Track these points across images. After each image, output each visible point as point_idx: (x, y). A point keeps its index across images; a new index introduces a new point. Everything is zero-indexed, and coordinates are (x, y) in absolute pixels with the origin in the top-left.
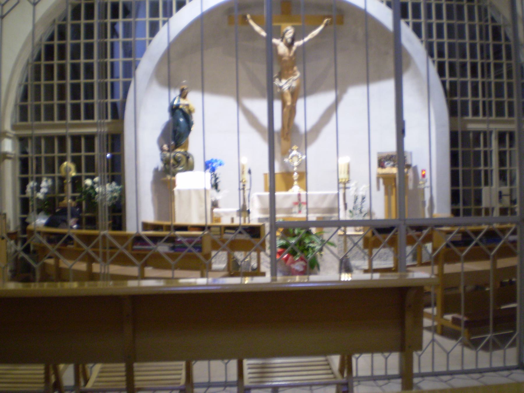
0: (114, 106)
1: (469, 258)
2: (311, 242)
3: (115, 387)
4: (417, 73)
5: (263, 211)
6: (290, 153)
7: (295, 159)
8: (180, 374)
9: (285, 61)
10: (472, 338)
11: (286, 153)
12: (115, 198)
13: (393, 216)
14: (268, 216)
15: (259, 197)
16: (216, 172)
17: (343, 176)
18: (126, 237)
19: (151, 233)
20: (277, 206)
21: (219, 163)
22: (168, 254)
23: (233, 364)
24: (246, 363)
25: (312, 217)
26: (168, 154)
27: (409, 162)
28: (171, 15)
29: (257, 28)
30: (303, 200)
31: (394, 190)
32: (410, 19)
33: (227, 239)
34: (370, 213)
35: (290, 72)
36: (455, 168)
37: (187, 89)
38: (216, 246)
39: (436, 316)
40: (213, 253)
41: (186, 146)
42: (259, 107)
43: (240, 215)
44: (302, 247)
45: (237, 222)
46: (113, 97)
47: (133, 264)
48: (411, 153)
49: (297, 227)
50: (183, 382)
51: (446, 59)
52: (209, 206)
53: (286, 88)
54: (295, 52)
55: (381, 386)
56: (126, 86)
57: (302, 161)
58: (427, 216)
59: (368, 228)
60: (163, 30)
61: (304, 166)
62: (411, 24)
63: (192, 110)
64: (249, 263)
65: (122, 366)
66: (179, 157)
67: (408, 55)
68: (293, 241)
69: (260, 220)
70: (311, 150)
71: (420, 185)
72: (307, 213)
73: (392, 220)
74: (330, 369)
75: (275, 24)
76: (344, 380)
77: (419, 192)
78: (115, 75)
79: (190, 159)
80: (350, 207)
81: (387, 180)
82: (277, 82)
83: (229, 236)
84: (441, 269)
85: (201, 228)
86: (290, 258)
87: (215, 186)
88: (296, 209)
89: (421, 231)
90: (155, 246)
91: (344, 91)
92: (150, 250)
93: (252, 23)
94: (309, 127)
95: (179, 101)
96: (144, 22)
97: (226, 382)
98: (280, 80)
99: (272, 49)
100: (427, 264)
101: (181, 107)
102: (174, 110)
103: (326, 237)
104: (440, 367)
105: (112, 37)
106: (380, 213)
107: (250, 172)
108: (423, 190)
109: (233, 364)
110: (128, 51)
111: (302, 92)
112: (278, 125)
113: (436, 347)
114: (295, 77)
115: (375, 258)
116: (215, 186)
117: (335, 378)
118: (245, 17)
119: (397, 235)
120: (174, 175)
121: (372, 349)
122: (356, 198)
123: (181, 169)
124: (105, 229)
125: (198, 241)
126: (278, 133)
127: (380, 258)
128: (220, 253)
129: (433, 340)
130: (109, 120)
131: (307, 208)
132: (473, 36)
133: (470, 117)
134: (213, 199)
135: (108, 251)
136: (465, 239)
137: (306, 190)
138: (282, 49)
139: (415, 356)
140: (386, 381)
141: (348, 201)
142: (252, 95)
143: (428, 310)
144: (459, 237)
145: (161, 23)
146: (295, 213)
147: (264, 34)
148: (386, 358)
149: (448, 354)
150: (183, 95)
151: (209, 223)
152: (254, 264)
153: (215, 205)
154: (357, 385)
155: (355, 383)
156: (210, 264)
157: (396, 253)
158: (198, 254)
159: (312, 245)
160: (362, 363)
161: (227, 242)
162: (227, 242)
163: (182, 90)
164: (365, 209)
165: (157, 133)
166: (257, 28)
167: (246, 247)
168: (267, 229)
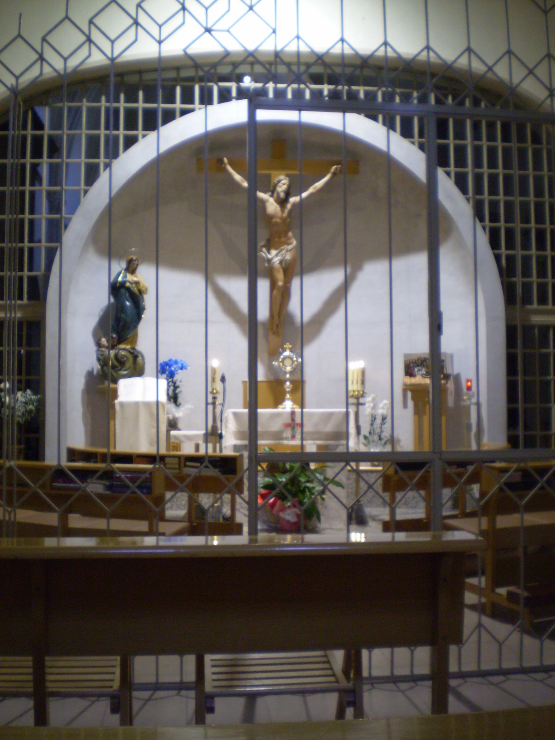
0: (33, 281)
1: (531, 507)
2: (308, 481)
3: (21, 690)
5: (239, 435)
6: (281, 354)
7: (288, 362)
8: (114, 673)
9: (276, 224)
10: (536, 621)
11: (274, 353)
12: (31, 411)
13: (427, 447)
14: (246, 442)
15: (235, 415)
16: (177, 378)
17: (354, 387)
18: (43, 470)
19: (80, 464)
20: (260, 429)
21: (180, 365)
22: (100, 496)
23: (190, 660)
24: (208, 658)
25: (311, 447)
26: (106, 351)
27: (448, 370)
28: (116, 155)
29: (238, 177)
30: (298, 420)
31: (428, 407)
32: (452, 169)
33: (189, 476)
34: (392, 440)
35: (283, 239)
37: (137, 260)
38: (171, 486)
40: (168, 495)
41: (134, 340)
42: (237, 288)
43: (206, 442)
44: (295, 490)
45: (202, 452)
46: (31, 269)
47: (50, 509)
48: (452, 356)
49: (288, 461)
50: (116, 684)
51: (502, 224)
52: (163, 427)
53: (276, 261)
54: (290, 212)
55: (403, 692)
56: (51, 254)
57: (297, 365)
58: (474, 447)
59: (389, 463)
60: (104, 176)
61: (299, 372)
62: (453, 175)
63: (143, 289)
64: (219, 509)
65: (28, 661)
66: (124, 356)
67: (448, 217)
68: (283, 479)
69: (236, 448)
70: (310, 351)
71: (464, 400)
72: (302, 439)
73: (425, 452)
74: (331, 669)
75: (261, 172)
76: (350, 685)
77: (461, 412)
78: (36, 238)
79: (140, 359)
80: (365, 431)
81: (417, 393)
82: (264, 253)
83: (192, 471)
84: (492, 522)
85: (150, 458)
86: (279, 502)
88: (288, 433)
89: (462, 468)
90: (83, 485)
91: (358, 268)
92: (77, 489)
94: (306, 318)
95: (125, 276)
96: (79, 165)
97: (181, 683)
98: (269, 251)
99: (257, 206)
100: (473, 514)
101: (128, 284)
102: (116, 289)
103: (330, 474)
104: (489, 665)
105: (32, 184)
106: (407, 443)
107: (223, 379)
108: (468, 408)
109: (190, 660)
110: (55, 204)
111: (298, 268)
112: (263, 312)
113: (484, 634)
114: (290, 247)
115: (399, 505)
116: (174, 398)
117: (337, 682)
118: (221, 161)
119: (430, 472)
120: (115, 381)
121: (390, 641)
123: (125, 373)
124: (13, 459)
125: (147, 478)
126: (264, 324)
127: (406, 504)
128: (179, 494)
129: (480, 625)
130: (25, 301)
131: (302, 433)
132: (539, 193)
133: (535, 306)
134: (171, 417)
135: (15, 489)
136: (526, 480)
137: (302, 406)
138: (272, 206)
139: (453, 649)
140: (412, 684)
141: (361, 423)
142: (229, 271)
143: (473, 581)
144: (518, 478)
145: (102, 167)
146: (287, 439)
147: (245, 184)
148: (412, 652)
149: (500, 644)
150: (131, 268)
151: (163, 451)
152: (226, 510)
153: (173, 425)
154: (370, 690)
155: (366, 687)
156: (163, 511)
157: (427, 500)
159: (308, 485)
160: (377, 660)
161: (188, 480)
162: (188, 480)
164: (386, 434)
165: (93, 321)
166: (238, 177)
167: (215, 487)
168: (246, 462)
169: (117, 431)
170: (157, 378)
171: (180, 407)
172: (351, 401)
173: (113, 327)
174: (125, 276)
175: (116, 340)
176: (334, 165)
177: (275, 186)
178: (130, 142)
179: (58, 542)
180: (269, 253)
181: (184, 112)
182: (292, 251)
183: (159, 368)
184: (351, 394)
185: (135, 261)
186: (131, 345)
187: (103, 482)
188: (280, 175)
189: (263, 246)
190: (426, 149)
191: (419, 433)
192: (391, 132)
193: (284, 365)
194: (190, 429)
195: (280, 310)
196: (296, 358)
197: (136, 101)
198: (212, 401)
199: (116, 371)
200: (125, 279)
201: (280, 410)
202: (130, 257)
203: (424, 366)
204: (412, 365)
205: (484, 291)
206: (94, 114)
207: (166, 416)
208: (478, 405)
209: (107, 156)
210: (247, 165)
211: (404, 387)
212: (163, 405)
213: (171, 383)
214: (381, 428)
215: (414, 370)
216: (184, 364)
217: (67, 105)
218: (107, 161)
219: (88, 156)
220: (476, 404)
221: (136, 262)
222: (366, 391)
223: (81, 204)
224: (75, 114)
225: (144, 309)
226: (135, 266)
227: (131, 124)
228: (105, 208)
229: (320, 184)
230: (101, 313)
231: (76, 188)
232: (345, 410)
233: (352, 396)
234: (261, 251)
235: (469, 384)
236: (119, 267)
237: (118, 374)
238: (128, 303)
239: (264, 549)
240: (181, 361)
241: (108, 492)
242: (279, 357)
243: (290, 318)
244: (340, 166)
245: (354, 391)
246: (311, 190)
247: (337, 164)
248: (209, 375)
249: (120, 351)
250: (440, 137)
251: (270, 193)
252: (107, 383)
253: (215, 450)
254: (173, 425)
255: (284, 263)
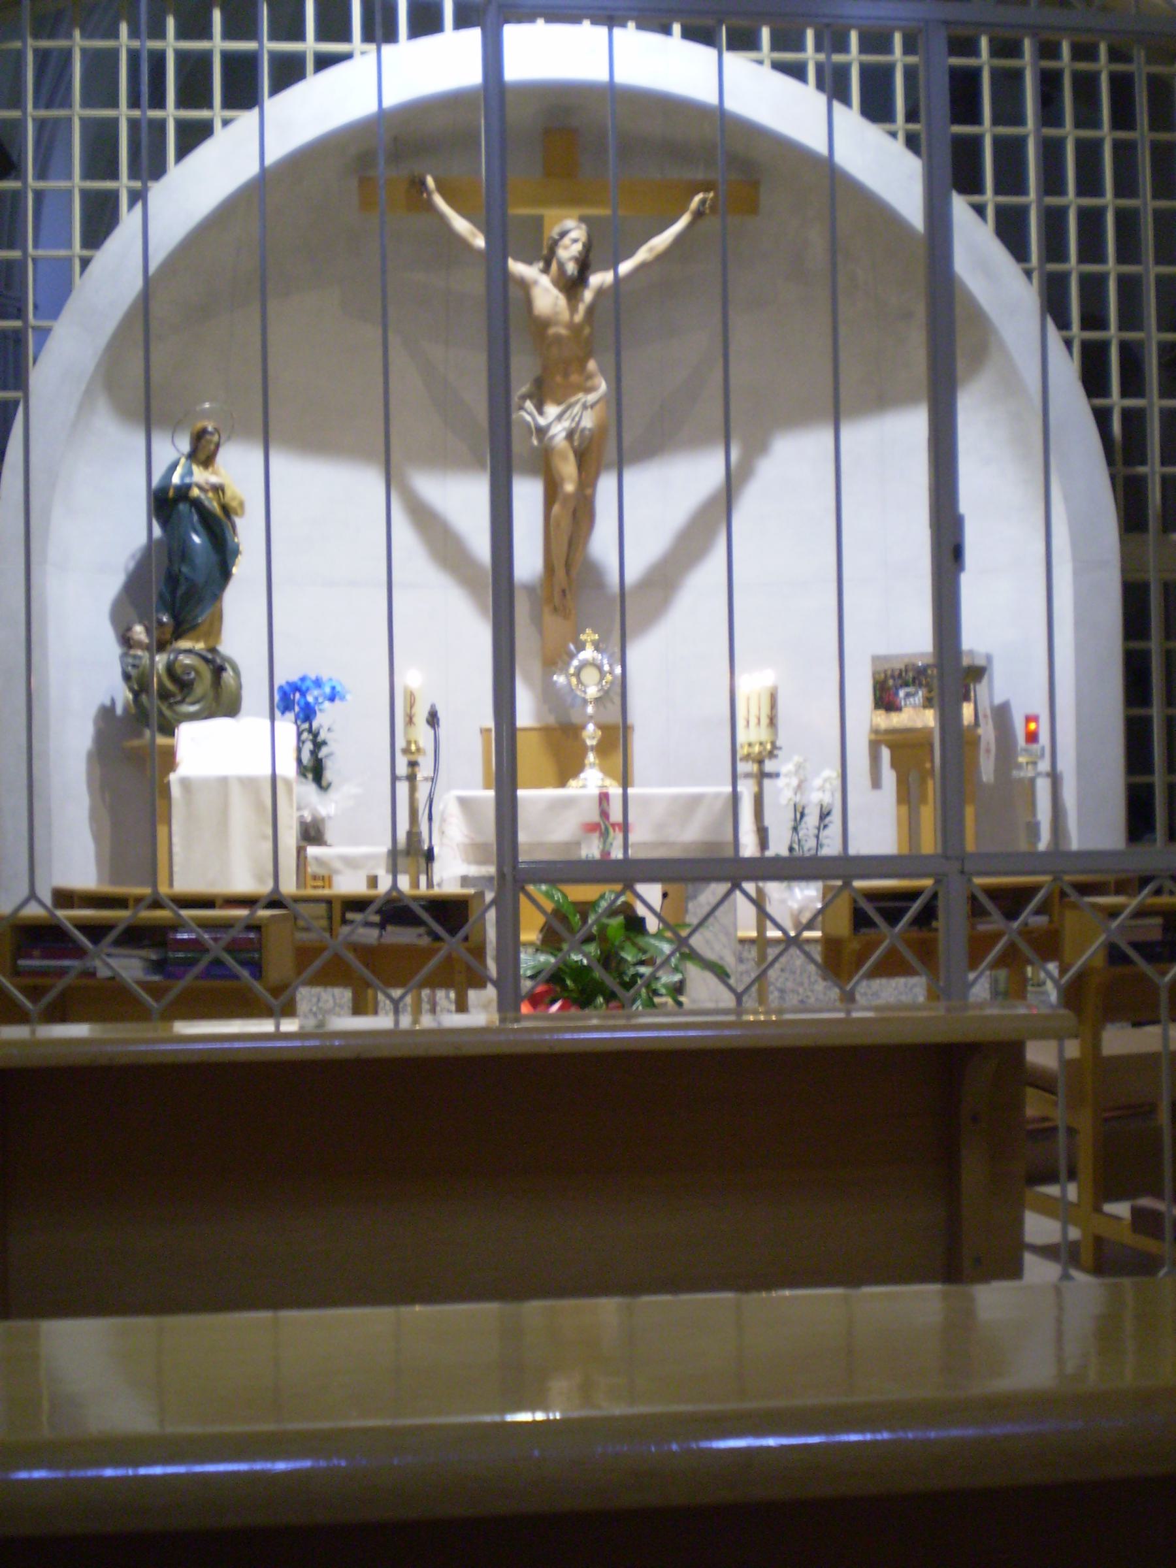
4: (1010, 383)
5: (476, 852)
6: (572, 656)
7: (590, 675)
9: (558, 339)
11: (555, 659)
14: (491, 870)
15: (464, 802)
17: (751, 735)
21: (327, 690)
28: (158, 171)
29: (461, 224)
30: (616, 815)
32: (989, 196)
35: (574, 378)
36: (1139, 711)
39: (1077, 1205)
42: (463, 500)
43: (394, 871)
51: (1113, 333)
52: (289, 838)
53: (559, 432)
61: (617, 700)
62: (990, 212)
63: (234, 504)
67: (978, 317)
69: (465, 881)
70: (644, 654)
71: (1019, 766)
75: (519, 211)
81: (903, 749)
82: (528, 413)
87: (315, 771)
89: (1015, 909)
91: (757, 447)
93: (439, 201)
94: (633, 574)
96: (69, 192)
99: (507, 298)
101: (195, 492)
102: (167, 503)
106: (876, 827)
107: (433, 719)
112: (528, 562)
114: (591, 398)
116: (315, 771)
120: (168, 729)
122: (800, 814)
123: (193, 709)
126: (530, 589)
138: (547, 297)
142: (443, 460)
147: (480, 242)
150: (203, 451)
151: (289, 886)
153: (312, 833)
158: (258, 986)
163: (199, 437)
165: (113, 584)
166: (461, 224)
169: (177, 859)
170: (273, 719)
171: (331, 791)
172: (743, 767)
173: (161, 596)
174: (190, 473)
175: (169, 631)
176: (698, 193)
177: (554, 244)
178: (194, 135)
179: (33, 1032)
180: (541, 412)
181: (324, 62)
182: (598, 407)
183: (277, 698)
184: (742, 751)
185: (211, 434)
186: (206, 642)
187: (144, 953)
188: (566, 217)
189: (524, 398)
190: (924, 149)
191: (910, 841)
192: (837, 105)
193: (579, 681)
194: (355, 842)
195: (568, 555)
196: (611, 666)
197: (207, 34)
198: (407, 772)
199: (171, 706)
200: (187, 480)
201: (573, 789)
202: (199, 425)
203: (920, 685)
204: (891, 682)
205: (1066, 498)
206: (101, 68)
207: (296, 815)
208: (1055, 777)
209: (134, 174)
210: (484, 191)
211: (873, 737)
212: (287, 782)
213: (305, 735)
214: (817, 837)
215: (897, 694)
216: (338, 688)
217: (31, 45)
218: (137, 184)
219: (89, 173)
220: (1048, 775)
221: (215, 438)
222: (778, 744)
223: (75, 294)
224: (53, 70)
225: (236, 552)
226: (212, 447)
227: (194, 92)
228: (137, 298)
229: (662, 240)
230: (132, 565)
231: (62, 253)
232: (729, 789)
233: (747, 757)
234: (521, 408)
235: (1032, 726)
236: (170, 450)
237: (175, 712)
238: (196, 539)
239: (535, 1037)
240: (331, 679)
241: (156, 978)
242: (568, 664)
243: (593, 573)
244: (711, 195)
245: (750, 745)
246: (643, 254)
247: (707, 190)
248: (397, 707)
249: (181, 657)
250: (957, 119)
251: (541, 265)
252: (148, 733)
253: (415, 884)
254: (312, 833)
255: (576, 437)
